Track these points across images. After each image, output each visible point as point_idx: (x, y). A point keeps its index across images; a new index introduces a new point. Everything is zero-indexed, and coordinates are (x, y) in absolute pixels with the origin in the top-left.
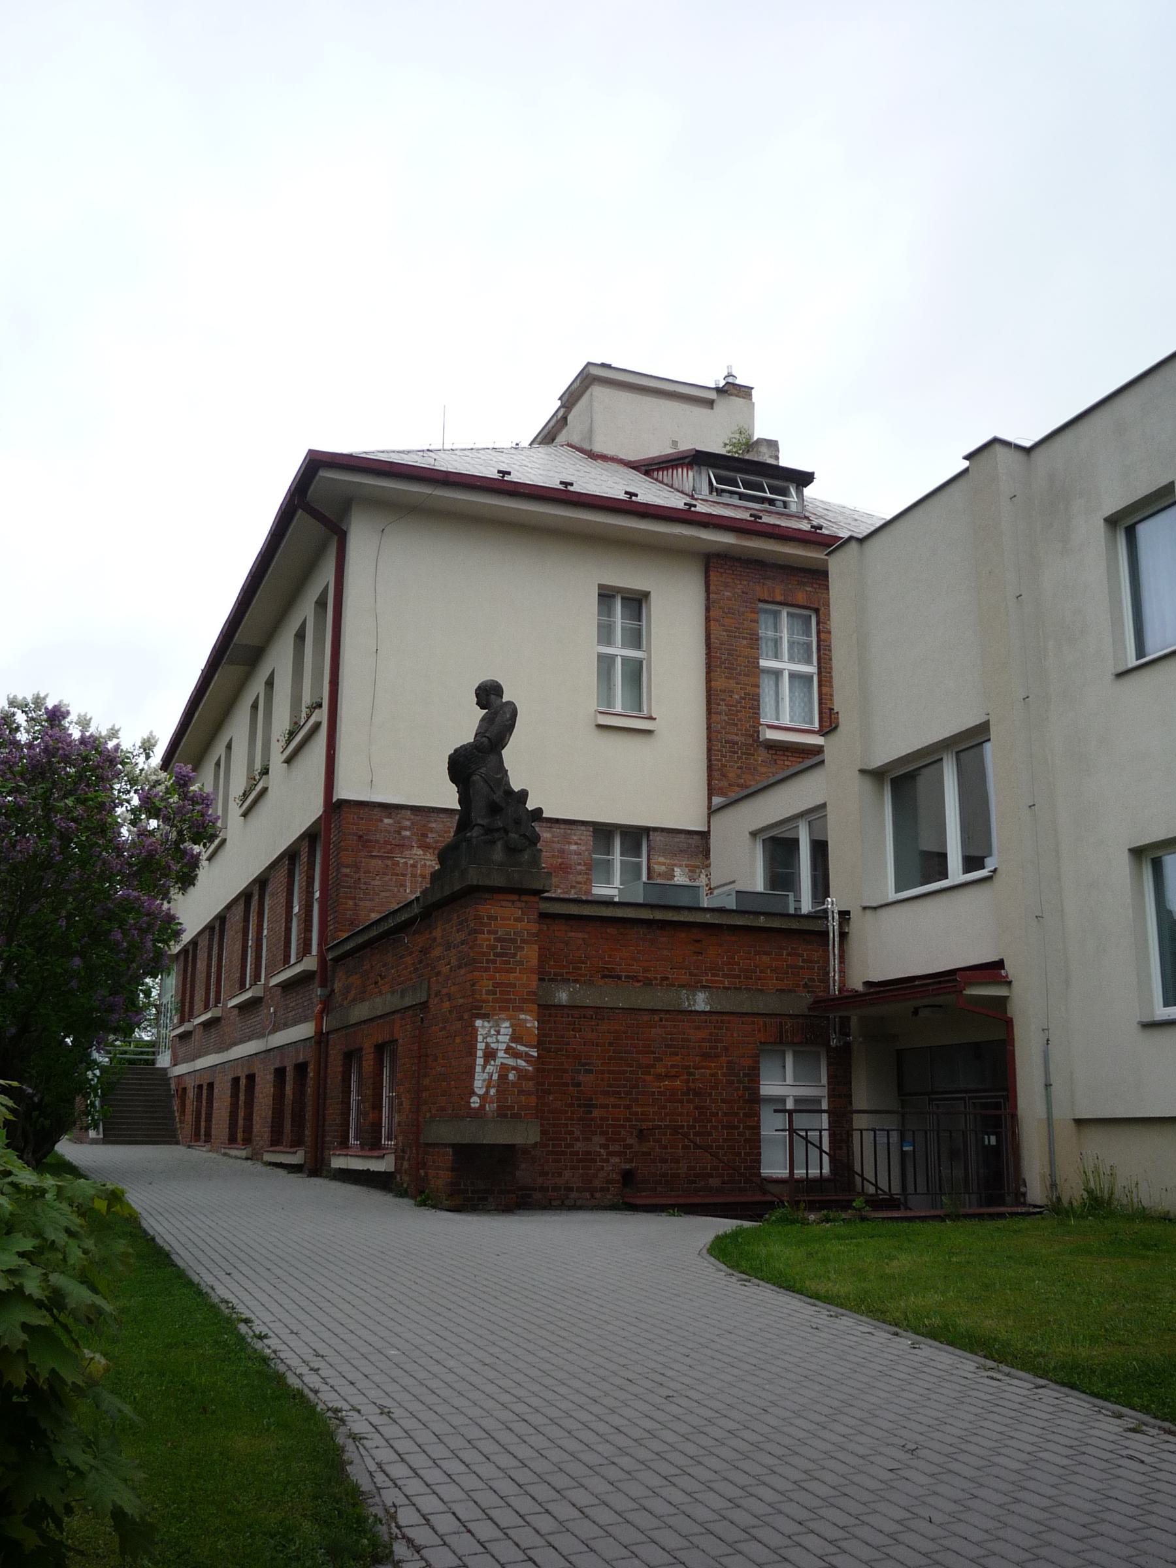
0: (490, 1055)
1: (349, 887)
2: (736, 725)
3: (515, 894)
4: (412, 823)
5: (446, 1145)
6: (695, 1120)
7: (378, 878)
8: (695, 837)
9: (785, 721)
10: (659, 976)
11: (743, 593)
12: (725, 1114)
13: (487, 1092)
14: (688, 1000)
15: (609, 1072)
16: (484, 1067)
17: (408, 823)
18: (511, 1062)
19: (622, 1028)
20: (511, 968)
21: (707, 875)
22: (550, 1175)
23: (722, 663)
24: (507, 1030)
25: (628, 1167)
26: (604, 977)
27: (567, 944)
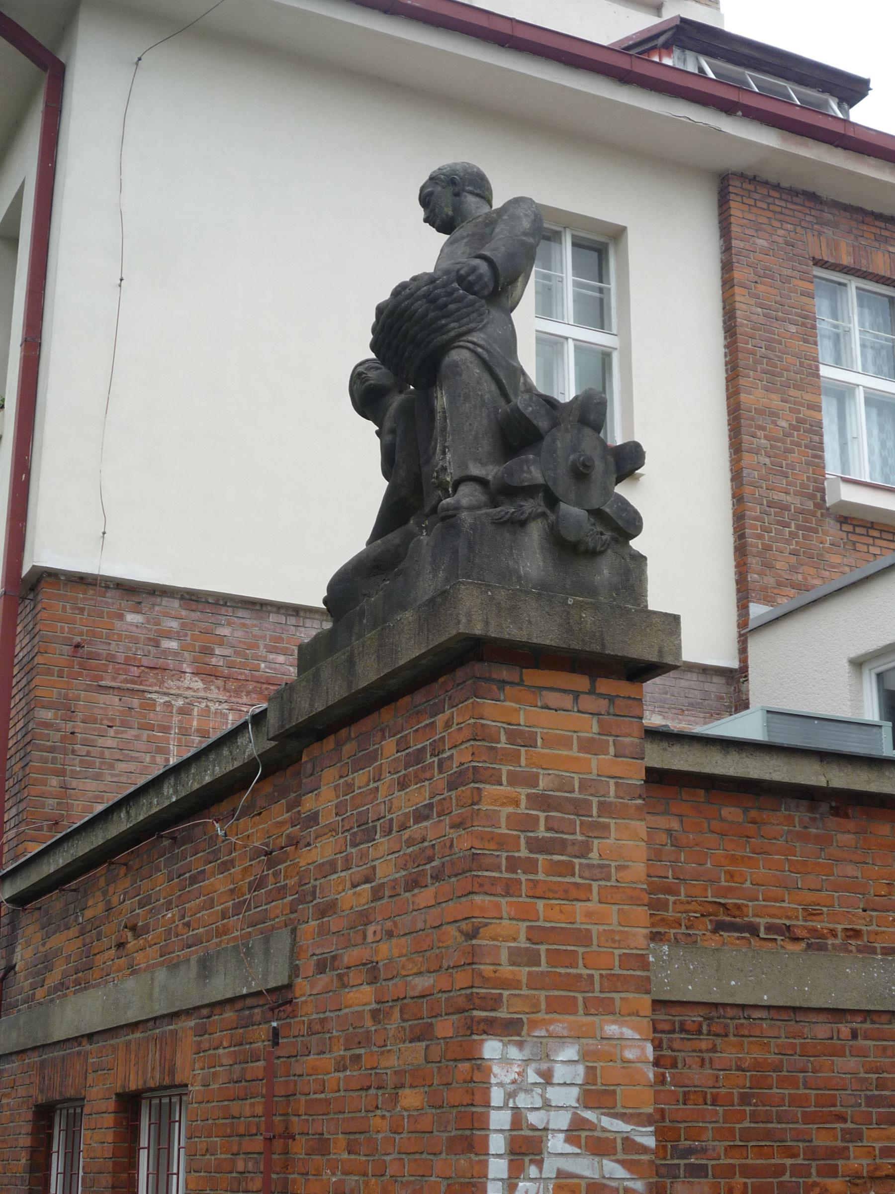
1: (52, 750)
3: (585, 674)
7: (111, 732)
8: (716, 679)
10: (839, 927)
11: (787, 243)
15: (747, 1171)
17: (174, 625)
19: (772, 1058)
23: (756, 362)
24: (570, 1069)
26: (719, 927)
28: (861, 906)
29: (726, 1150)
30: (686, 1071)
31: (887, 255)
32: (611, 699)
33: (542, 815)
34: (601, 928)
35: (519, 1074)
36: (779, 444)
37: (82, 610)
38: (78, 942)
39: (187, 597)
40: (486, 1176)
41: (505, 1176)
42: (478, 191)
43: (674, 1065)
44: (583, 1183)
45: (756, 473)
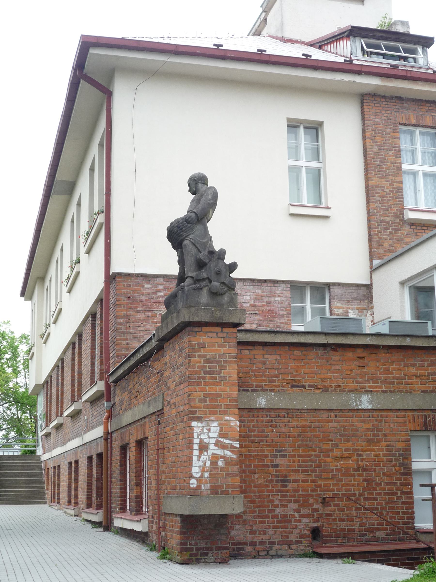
0: (203, 447)
1: (123, 332)
2: (388, 210)
4: (165, 287)
5: (176, 515)
6: (364, 489)
7: (142, 325)
8: (362, 288)
9: (422, 205)
10: (333, 385)
11: (388, 119)
12: (387, 484)
13: (202, 475)
14: (356, 401)
15: (299, 456)
16: (199, 457)
17: (161, 287)
18: (220, 452)
19: (308, 424)
20: (217, 382)
21: (371, 315)
22: (258, 533)
23: (376, 168)
24: (216, 428)
25: (315, 525)
26: (292, 386)
27: (264, 364)
28: (341, 378)
29: (293, 450)
30: (280, 428)
31: (431, 117)
32: (227, 333)
33: (208, 365)
34: (224, 392)
35: (201, 430)
36: (385, 198)
37: (130, 285)
38: (128, 396)
39: (165, 277)
40: (193, 455)
41: (198, 454)
42: (202, 182)
43: (276, 426)
44: (219, 456)
45: (375, 210)
